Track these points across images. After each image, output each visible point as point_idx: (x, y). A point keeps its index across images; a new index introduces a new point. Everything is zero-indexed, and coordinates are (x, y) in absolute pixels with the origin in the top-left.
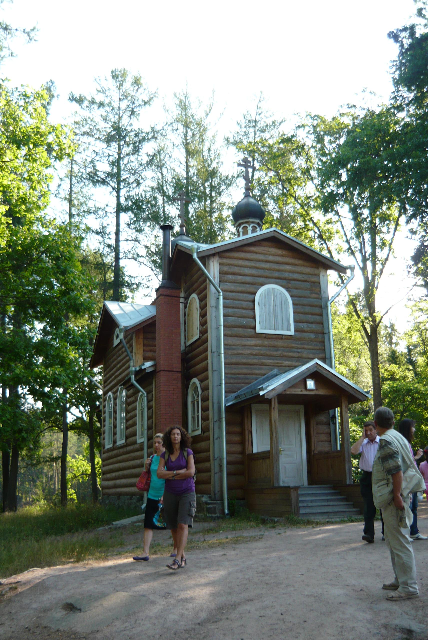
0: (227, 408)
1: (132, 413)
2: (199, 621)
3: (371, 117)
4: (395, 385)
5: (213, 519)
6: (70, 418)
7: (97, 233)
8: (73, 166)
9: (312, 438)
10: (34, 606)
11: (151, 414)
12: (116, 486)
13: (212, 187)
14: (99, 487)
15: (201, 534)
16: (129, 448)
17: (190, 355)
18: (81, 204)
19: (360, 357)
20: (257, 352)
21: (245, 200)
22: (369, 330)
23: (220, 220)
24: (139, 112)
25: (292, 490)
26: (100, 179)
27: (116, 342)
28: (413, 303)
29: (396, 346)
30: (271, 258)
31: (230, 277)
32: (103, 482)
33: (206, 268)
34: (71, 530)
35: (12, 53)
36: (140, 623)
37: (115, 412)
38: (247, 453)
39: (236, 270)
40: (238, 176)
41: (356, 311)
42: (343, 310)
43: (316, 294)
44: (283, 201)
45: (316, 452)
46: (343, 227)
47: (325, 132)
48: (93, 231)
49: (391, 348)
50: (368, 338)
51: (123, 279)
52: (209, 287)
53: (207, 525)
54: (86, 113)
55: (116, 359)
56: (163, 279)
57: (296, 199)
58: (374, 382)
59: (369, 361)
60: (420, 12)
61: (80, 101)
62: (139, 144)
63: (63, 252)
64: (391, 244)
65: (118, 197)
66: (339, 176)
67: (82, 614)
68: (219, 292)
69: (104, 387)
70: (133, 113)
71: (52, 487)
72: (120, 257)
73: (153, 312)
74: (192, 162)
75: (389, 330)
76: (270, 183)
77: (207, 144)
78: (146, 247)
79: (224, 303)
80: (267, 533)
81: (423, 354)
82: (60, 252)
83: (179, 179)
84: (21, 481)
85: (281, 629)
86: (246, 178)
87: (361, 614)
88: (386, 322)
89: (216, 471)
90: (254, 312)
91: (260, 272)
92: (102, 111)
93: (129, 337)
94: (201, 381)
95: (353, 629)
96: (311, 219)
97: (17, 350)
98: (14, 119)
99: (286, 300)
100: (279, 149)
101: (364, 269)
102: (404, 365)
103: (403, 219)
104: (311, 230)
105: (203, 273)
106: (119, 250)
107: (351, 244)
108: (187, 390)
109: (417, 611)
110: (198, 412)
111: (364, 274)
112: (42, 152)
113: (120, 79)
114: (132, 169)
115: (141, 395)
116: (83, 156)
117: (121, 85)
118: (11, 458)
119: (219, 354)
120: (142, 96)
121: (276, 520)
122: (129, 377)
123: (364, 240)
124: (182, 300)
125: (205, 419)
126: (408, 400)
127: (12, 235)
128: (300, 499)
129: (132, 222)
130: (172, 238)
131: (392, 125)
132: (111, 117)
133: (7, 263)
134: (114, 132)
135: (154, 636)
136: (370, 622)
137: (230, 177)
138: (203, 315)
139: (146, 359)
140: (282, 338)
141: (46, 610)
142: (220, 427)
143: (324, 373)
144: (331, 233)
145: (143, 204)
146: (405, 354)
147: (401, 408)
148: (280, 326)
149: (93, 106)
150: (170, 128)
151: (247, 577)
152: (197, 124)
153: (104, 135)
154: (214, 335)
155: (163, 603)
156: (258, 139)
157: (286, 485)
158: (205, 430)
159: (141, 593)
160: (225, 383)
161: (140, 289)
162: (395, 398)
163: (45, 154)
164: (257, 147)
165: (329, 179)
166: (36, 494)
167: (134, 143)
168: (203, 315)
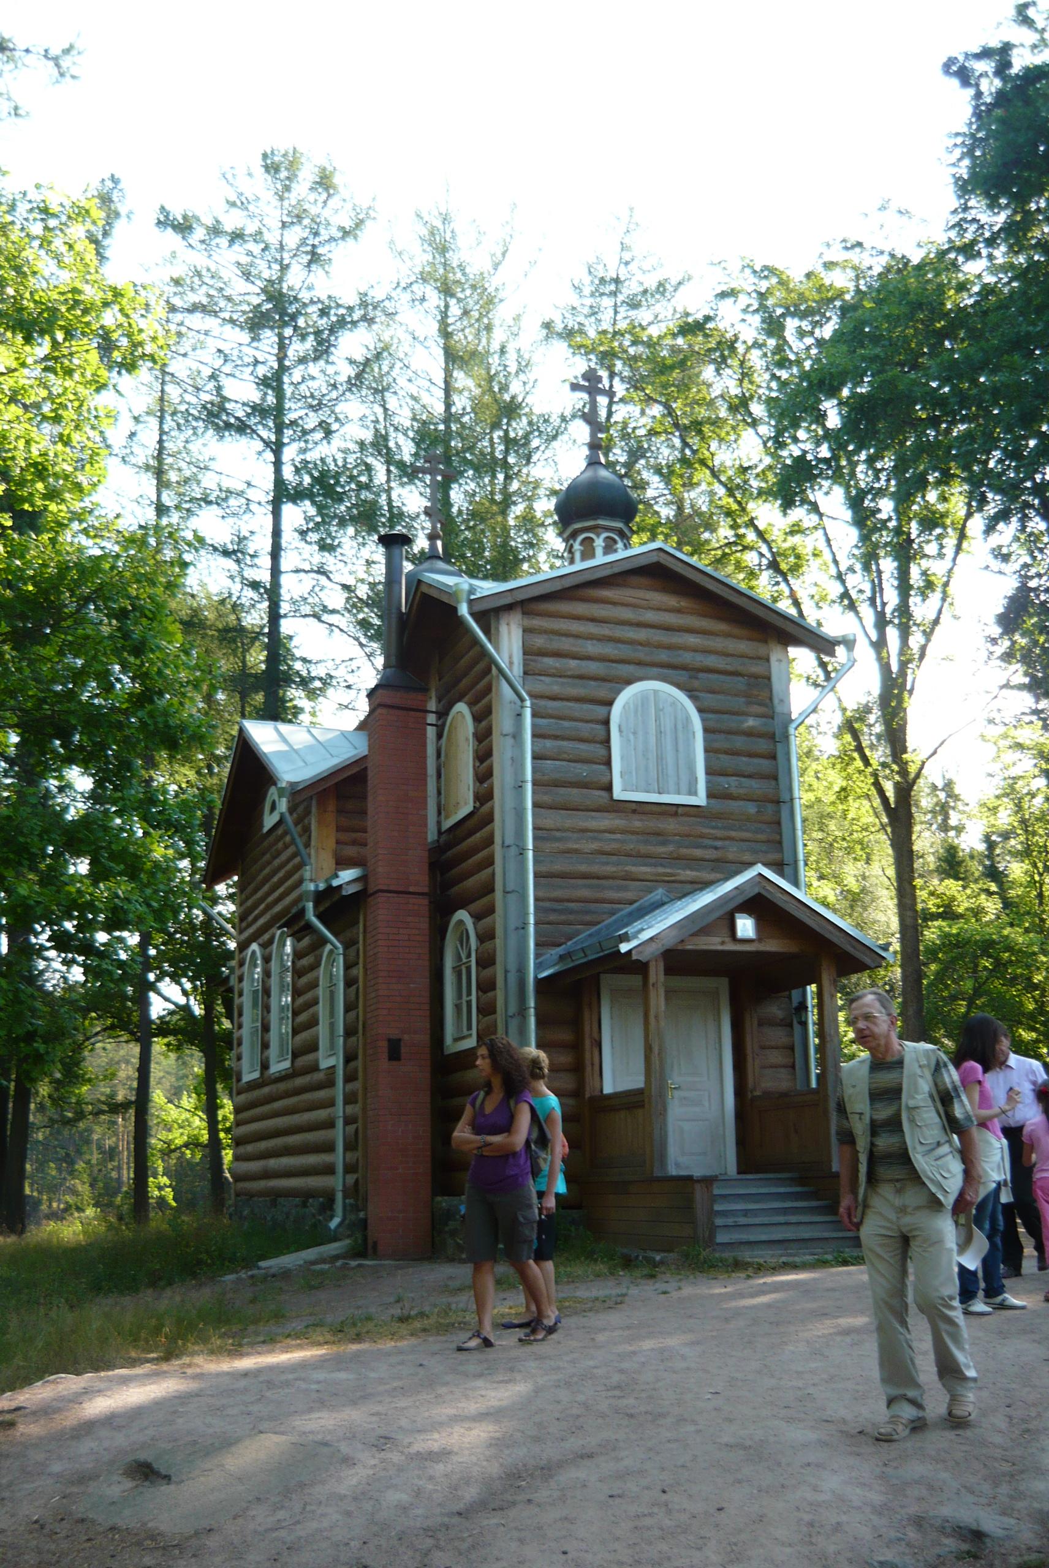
0: (539, 982)
2: (460, 1506)
4: (954, 931)
6: (157, 1008)
7: (226, 553)
8: (167, 388)
10: (56, 1468)
12: (267, 1175)
13: (508, 441)
14: (228, 1175)
16: (299, 1081)
17: (449, 854)
18: (187, 481)
19: (868, 861)
20: (615, 846)
22: (890, 793)
23: (529, 522)
24: (329, 255)
25: (698, 1186)
26: (232, 420)
27: (269, 821)
28: (1001, 729)
30: (650, 616)
31: (549, 662)
33: (490, 640)
34: (157, 1281)
35: (16, 108)
36: (313, 1512)
37: (267, 992)
38: (587, 1095)
39: (565, 644)
41: (859, 749)
42: (829, 745)
43: (760, 705)
44: (681, 476)
45: (757, 1093)
46: (828, 540)
47: (787, 309)
48: (215, 549)
50: (889, 816)
51: (290, 667)
54: (199, 259)
55: (269, 863)
57: (715, 474)
59: (891, 872)
61: (183, 227)
63: (137, 598)
64: (946, 584)
65: (278, 464)
66: (820, 418)
67: (172, 1487)
68: (522, 700)
69: (241, 932)
70: (315, 257)
71: (114, 1174)
72: (282, 612)
73: (360, 747)
74: (461, 379)
75: (942, 796)
76: (652, 433)
77: (498, 336)
78: (346, 587)
79: (534, 726)
80: (634, 1291)
81: (1026, 853)
82: (129, 597)
84: (37, 1160)
85: (662, 1529)
86: (590, 417)
87: (858, 1491)
88: (933, 774)
90: (609, 749)
91: (624, 651)
92: (238, 253)
93: (301, 809)
94: (477, 917)
95: (838, 1527)
96: (751, 523)
97: (21, 839)
98: (17, 269)
99: (688, 719)
101: (880, 645)
102: (976, 881)
103: (977, 524)
104: (752, 548)
105: (484, 653)
106: (279, 595)
107: (849, 585)
108: (443, 938)
109: (996, 1484)
110: (469, 994)
111: (880, 658)
113: (283, 174)
114: (312, 396)
115: (331, 952)
117: (287, 188)
119: (522, 852)
120: (337, 214)
121: (658, 1258)
122: (300, 906)
123: (879, 572)
125: (487, 1009)
128: (717, 1207)
129: (311, 525)
130: (408, 566)
131: (952, 292)
132: (260, 268)
134: (270, 306)
136: (879, 1511)
138: (484, 755)
139: (342, 863)
140: (676, 814)
141: (83, 1479)
144: (798, 557)
145: (337, 483)
146: (981, 854)
147: (968, 985)
149: (218, 240)
150: (407, 296)
151: (581, 1398)
152: (474, 287)
153: (244, 312)
154: (510, 804)
155: (373, 1462)
156: (622, 325)
160: (536, 924)
161: (330, 692)
162: (954, 960)
164: (621, 345)
165: (795, 425)
166: (74, 1192)
167: (318, 333)
168: (484, 755)
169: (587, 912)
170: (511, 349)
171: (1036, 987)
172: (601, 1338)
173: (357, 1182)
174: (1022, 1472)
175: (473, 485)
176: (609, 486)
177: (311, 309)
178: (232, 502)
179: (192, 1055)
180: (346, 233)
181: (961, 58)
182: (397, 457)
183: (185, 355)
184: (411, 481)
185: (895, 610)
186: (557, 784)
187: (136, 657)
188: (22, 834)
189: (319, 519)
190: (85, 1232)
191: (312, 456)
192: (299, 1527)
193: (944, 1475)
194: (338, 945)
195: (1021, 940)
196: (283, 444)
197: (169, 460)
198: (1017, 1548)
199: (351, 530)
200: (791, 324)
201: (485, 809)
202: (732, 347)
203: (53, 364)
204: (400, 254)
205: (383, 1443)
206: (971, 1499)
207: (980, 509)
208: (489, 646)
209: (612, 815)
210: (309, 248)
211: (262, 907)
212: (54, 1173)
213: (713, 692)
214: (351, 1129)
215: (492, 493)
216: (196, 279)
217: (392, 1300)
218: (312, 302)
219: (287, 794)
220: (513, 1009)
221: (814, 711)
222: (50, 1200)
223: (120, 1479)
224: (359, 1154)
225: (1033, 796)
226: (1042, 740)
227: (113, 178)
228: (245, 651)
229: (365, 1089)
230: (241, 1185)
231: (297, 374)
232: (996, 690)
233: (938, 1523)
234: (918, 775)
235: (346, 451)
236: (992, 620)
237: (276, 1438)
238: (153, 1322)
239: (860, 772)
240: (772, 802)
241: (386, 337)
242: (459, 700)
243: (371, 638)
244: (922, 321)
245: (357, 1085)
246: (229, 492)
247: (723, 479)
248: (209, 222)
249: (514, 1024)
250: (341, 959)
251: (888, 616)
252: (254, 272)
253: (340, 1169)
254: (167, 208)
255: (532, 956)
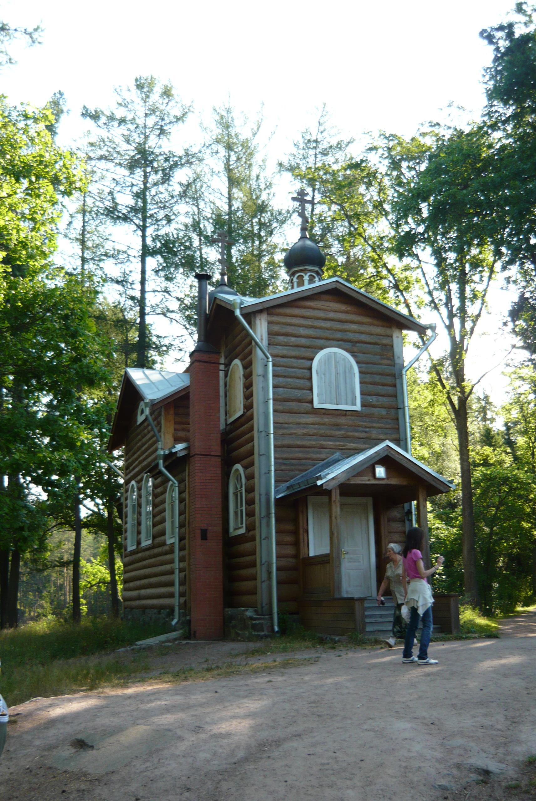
0: (277, 500)
1: (160, 508)
2: (235, 760)
3: (459, 137)
4: (489, 472)
5: (260, 638)
6: (84, 513)
7: (118, 282)
8: (86, 199)
9: (383, 538)
10: (37, 743)
11: (183, 508)
12: (140, 598)
13: (262, 225)
14: (120, 598)
15: (244, 656)
16: (156, 551)
17: (231, 435)
18: (97, 246)
19: (445, 436)
20: (314, 431)
21: (301, 243)
22: (456, 402)
23: (272, 264)
24: (169, 130)
25: (357, 603)
26: (120, 215)
27: (140, 419)
28: (513, 369)
29: (492, 422)
30: (332, 315)
31: (281, 338)
32: (125, 593)
33: (251, 328)
34: (86, 652)
35: (10, 59)
36: (163, 763)
37: (140, 505)
38: (301, 557)
39: (289, 330)
40: (293, 212)
41: (440, 380)
42: (425, 378)
43: (388, 359)
44: (349, 242)
46: (424, 274)
47: (402, 156)
48: (112, 280)
49: (485, 426)
50: (455, 414)
51: (150, 340)
52: (255, 351)
53: (252, 646)
54: (104, 133)
55: (140, 440)
56: (199, 340)
57: (365, 240)
58: (462, 468)
59: (457, 442)
60: (519, 8)
61: (95, 117)
62: (170, 171)
63: (73, 309)
64: (484, 296)
65: (144, 237)
66: (420, 211)
67: (94, 751)
68: (268, 358)
69: (126, 475)
70: (162, 131)
71: (62, 598)
72: (146, 312)
73: (185, 382)
74: (236, 192)
75: (483, 403)
76: (334, 220)
77: (255, 171)
78: (178, 299)
79: (273, 371)
80: (324, 655)
81: (525, 432)
82: (69, 309)
83: (219, 216)
84: (23, 591)
85: (333, 770)
86: (302, 215)
87: (430, 751)
88: (478, 392)
89: (263, 580)
90: (311, 382)
91: (319, 333)
92: (123, 130)
93: (156, 413)
94: (245, 467)
95: (419, 769)
96: (385, 265)
97: (16, 430)
98: (12, 145)
99: (351, 367)
100: (346, 177)
101: (450, 327)
102: (500, 447)
103: (498, 266)
104: (385, 278)
105: (248, 334)
106: (144, 303)
107: (434, 297)
108: (228, 478)
109: (497, 748)
110: (242, 506)
111: (450, 334)
112: (47, 188)
113: (146, 89)
114: (161, 202)
115: (172, 485)
116: (99, 185)
117: (148, 97)
118: (10, 558)
119: (268, 435)
120: (174, 110)
121: (337, 639)
122: (156, 462)
123: (450, 290)
124: (222, 367)
125: (250, 514)
126: (505, 491)
127: (10, 288)
128: (366, 613)
129: (161, 268)
130: (210, 289)
131: (485, 149)
132: (134, 137)
133: (4, 323)
134: (139, 156)
135: (180, 778)
136: (439, 761)
137: (284, 212)
138: (248, 386)
139: (177, 440)
140: (345, 415)
141: (50, 748)
142: (268, 525)
143: (397, 458)
144: (408, 283)
145: (174, 246)
146: (503, 432)
147: (496, 500)
148: (343, 398)
149: (112, 123)
150: (208, 151)
151: (295, 707)
152: (242, 145)
153: (126, 159)
154: (261, 410)
155: (193, 739)
156: (319, 165)
157: (350, 596)
158: (251, 528)
159: (166, 727)
160: (275, 471)
161: (171, 352)
162: (489, 487)
163: (51, 188)
164: (318, 174)
165: (406, 216)
166: (42, 607)
167: (164, 170)
168: (248, 386)
169: (301, 465)
170: (261, 177)
171: (531, 501)
172: (307, 678)
173: (185, 601)
174: (510, 742)
175: (243, 247)
176: (311, 249)
177: (160, 158)
178: (120, 256)
179: (101, 537)
180: (178, 119)
181: (489, 30)
182: (205, 233)
183: (96, 181)
184: (211, 245)
185: (457, 310)
186: (285, 400)
187: (73, 339)
188: (16, 427)
189: (165, 265)
190: (48, 627)
191: (162, 232)
192: (156, 770)
193: (472, 744)
194: (176, 482)
195: (522, 476)
196: (147, 227)
197: (88, 236)
198: (506, 778)
199: (181, 270)
200: (404, 164)
201: (249, 412)
202: (375, 177)
203: (31, 192)
204: (205, 129)
205: (198, 729)
206: (485, 755)
207: (500, 258)
208: (251, 331)
209: (314, 416)
210: (159, 127)
211: (137, 462)
212: (31, 597)
213: (364, 353)
214: (183, 574)
215: (253, 251)
216: (102, 143)
217: (203, 660)
218: (161, 154)
219: (149, 405)
220: (264, 514)
221: (417, 360)
222: (30, 611)
223: (69, 748)
224: (186, 587)
225: (529, 403)
226: (533, 375)
227: (61, 94)
228: (128, 331)
229: (189, 554)
230: (127, 603)
231: (153, 191)
232: (510, 349)
233: (468, 767)
234: (470, 393)
235: (178, 230)
236: (507, 314)
237: (145, 727)
238: (85, 672)
239: (441, 392)
240: (394, 408)
241: (198, 171)
242: (236, 358)
243: (192, 325)
244: (470, 164)
245: (185, 552)
246: (119, 251)
247: (370, 242)
248: (108, 113)
249: (264, 521)
250: (177, 488)
251: (455, 312)
252: (131, 139)
253: (177, 595)
254: (87, 107)
255: (273, 487)
